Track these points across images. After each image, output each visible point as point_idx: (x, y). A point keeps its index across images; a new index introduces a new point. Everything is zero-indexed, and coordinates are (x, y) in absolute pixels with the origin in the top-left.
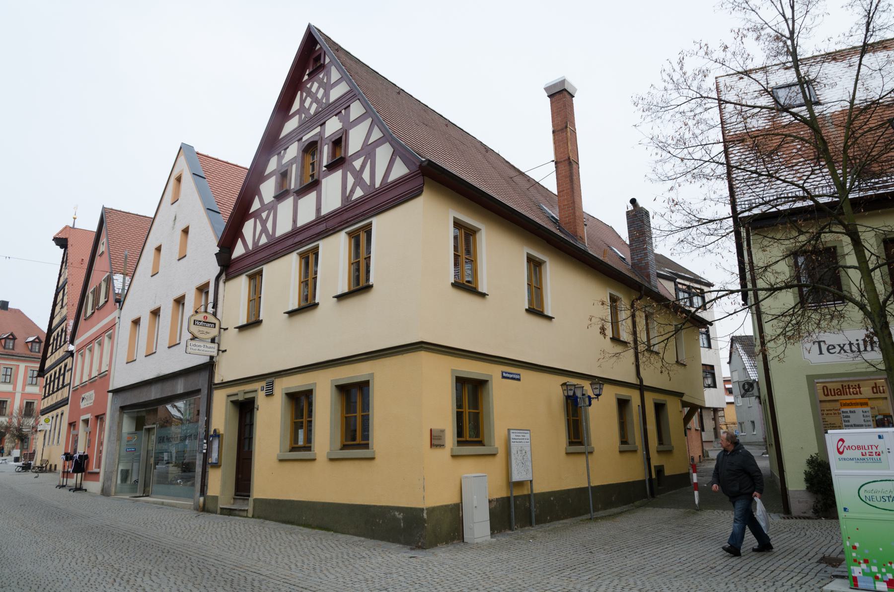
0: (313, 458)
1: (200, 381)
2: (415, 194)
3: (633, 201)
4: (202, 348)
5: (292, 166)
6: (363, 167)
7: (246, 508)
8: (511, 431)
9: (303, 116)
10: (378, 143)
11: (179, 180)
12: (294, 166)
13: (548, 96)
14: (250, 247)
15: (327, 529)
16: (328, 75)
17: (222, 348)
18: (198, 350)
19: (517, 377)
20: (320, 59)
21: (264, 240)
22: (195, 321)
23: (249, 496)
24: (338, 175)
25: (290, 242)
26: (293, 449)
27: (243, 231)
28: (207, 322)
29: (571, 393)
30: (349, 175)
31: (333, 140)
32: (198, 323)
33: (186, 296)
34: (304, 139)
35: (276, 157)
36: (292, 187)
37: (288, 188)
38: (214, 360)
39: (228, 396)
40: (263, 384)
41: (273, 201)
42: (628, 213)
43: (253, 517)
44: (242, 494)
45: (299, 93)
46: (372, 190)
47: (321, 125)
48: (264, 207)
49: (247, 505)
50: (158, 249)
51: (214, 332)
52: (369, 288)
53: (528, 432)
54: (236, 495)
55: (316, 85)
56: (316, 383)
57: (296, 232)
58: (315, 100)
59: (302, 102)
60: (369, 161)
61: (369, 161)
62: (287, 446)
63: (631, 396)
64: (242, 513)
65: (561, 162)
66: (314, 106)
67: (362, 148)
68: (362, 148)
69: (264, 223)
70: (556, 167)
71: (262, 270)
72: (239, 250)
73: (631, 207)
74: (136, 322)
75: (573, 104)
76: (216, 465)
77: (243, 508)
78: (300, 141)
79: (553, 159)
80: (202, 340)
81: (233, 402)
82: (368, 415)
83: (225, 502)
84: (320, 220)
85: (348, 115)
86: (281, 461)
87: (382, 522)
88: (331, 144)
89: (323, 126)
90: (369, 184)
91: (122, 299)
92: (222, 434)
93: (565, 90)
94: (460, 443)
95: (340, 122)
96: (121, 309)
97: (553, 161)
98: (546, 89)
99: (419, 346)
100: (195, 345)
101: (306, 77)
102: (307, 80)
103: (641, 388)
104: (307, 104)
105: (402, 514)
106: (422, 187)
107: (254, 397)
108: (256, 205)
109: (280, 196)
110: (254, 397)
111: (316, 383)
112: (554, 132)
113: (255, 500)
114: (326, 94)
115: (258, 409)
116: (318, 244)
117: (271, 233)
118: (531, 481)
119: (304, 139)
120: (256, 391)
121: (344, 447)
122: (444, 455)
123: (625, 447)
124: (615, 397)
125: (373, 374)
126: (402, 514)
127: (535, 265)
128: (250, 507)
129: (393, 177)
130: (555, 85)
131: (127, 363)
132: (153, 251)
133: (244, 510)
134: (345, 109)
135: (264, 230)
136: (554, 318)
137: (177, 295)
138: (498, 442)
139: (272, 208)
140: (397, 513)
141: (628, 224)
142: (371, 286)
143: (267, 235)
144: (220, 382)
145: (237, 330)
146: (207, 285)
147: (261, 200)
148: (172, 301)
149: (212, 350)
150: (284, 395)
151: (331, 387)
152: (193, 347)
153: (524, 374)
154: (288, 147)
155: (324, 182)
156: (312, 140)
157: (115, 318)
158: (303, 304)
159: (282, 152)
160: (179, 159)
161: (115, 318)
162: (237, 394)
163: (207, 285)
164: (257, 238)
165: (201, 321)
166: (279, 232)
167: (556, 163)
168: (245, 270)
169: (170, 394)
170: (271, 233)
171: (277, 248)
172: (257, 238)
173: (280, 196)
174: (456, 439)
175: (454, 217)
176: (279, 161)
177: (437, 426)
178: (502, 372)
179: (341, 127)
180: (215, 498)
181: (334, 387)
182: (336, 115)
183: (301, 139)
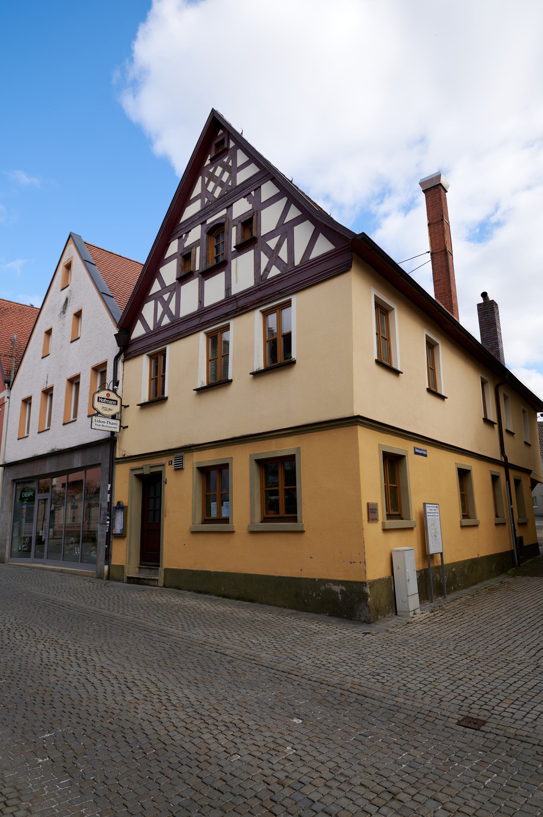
0: (231, 530)
1: (102, 456)
2: (343, 269)
3: (484, 295)
4: (106, 424)
5: (196, 248)
6: (279, 246)
7: (157, 578)
8: (427, 505)
9: (206, 200)
10: (297, 221)
11: (68, 267)
12: (198, 249)
13: (423, 191)
14: (152, 328)
16: (234, 158)
17: (124, 425)
18: (103, 426)
19: (424, 453)
20: (224, 143)
21: (166, 321)
22: (98, 398)
23: (159, 566)
24: (249, 256)
25: (196, 322)
26: (205, 521)
27: (142, 312)
28: (110, 400)
29: (271, 478)
30: (263, 255)
31: (243, 221)
32: (102, 400)
33: (81, 376)
34: (209, 222)
35: (177, 241)
36: (197, 268)
37: (192, 269)
38: (115, 435)
39: (132, 470)
40: (172, 458)
41: (175, 283)
42: (479, 305)
43: (164, 586)
44: (148, 563)
45: (200, 178)
46: (290, 268)
47: (227, 208)
48: (165, 288)
49: (157, 574)
50: (49, 333)
51: (116, 409)
52: (290, 363)
53: (438, 506)
54: (141, 564)
55: (219, 170)
56: (232, 457)
57: (202, 311)
58: (219, 183)
59: (205, 186)
60: (286, 240)
61: (286, 240)
62: (199, 517)
63: (499, 473)
64: (152, 583)
65: (437, 252)
66: (219, 190)
67: (277, 228)
68: (276, 227)
69: (166, 305)
70: (431, 258)
71: (166, 350)
72: (138, 331)
73: (481, 301)
74: (27, 401)
75: (446, 198)
76: (122, 536)
77: (153, 578)
78: (204, 225)
79: (429, 249)
80: (105, 416)
81: (136, 476)
82: (295, 489)
83: (132, 571)
84: (230, 299)
85: (259, 196)
86: (193, 532)
88: (240, 225)
89: (229, 209)
90: (286, 262)
91: (12, 380)
92: (127, 507)
93: (441, 184)
95: (250, 203)
96: (11, 389)
97: (428, 252)
98: (421, 184)
99: (354, 420)
100: (99, 421)
101: (208, 162)
102: (209, 164)
103: (506, 465)
104: (210, 188)
106: (351, 263)
107: (161, 471)
108: (156, 287)
109: (183, 279)
110: (161, 471)
111: (232, 457)
112: (429, 225)
113: (166, 570)
114: (233, 177)
115: (166, 483)
116: (229, 323)
117: (174, 314)
118: (441, 554)
119: (209, 222)
120: (164, 465)
121: (265, 520)
122: (377, 527)
123: (467, 522)
124: (489, 473)
125: (299, 449)
127: (431, 346)
128: (161, 577)
129: (315, 253)
130: (430, 180)
131: (18, 439)
132: (43, 334)
133: (154, 580)
134: (255, 190)
135: (167, 311)
137: (72, 374)
138: (414, 517)
139: (175, 289)
141: (479, 316)
142: (294, 363)
143: (170, 315)
144: (121, 456)
145: (139, 407)
146: (105, 364)
147: (162, 282)
148: (65, 381)
149: (114, 426)
150: (195, 470)
151: (250, 460)
152: (97, 423)
153: (431, 451)
154: (190, 231)
155: (233, 262)
156: (218, 222)
157: (4, 397)
158: (212, 381)
159: (184, 236)
160: (68, 248)
161: (4, 397)
162: (142, 468)
163: (105, 364)
164: (158, 318)
165: (104, 399)
166: (183, 314)
167: (431, 254)
168: (146, 350)
169: (66, 468)
170: (174, 314)
171: (183, 328)
172: (158, 318)
173: (183, 279)
175: (375, 295)
176: (180, 245)
177: (372, 501)
178: (415, 448)
179: (251, 208)
180: (122, 568)
181: (254, 463)
182: (244, 197)
183: (205, 221)
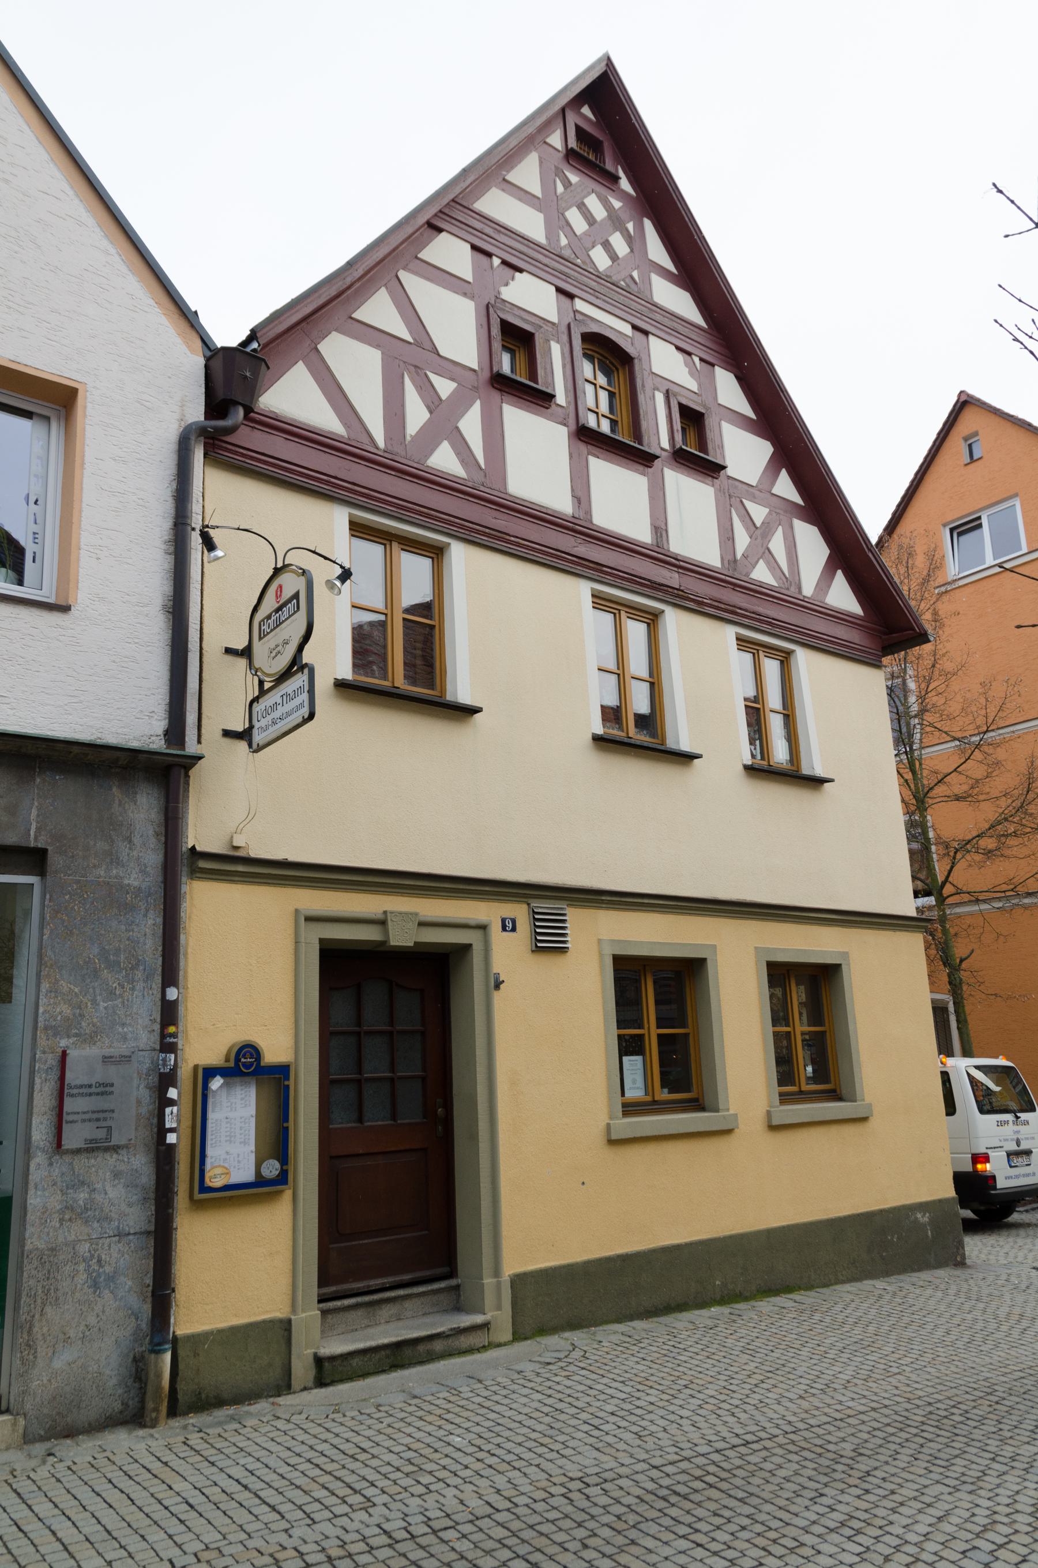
15: (786, 1289)
18: (274, 723)
43: (518, 1336)
87: (898, 1238)
94: (785, 1098)
105: (927, 1215)
126: (927, 1215)
136: (698, 756)
140: (919, 1216)
174: (776, 1089)
